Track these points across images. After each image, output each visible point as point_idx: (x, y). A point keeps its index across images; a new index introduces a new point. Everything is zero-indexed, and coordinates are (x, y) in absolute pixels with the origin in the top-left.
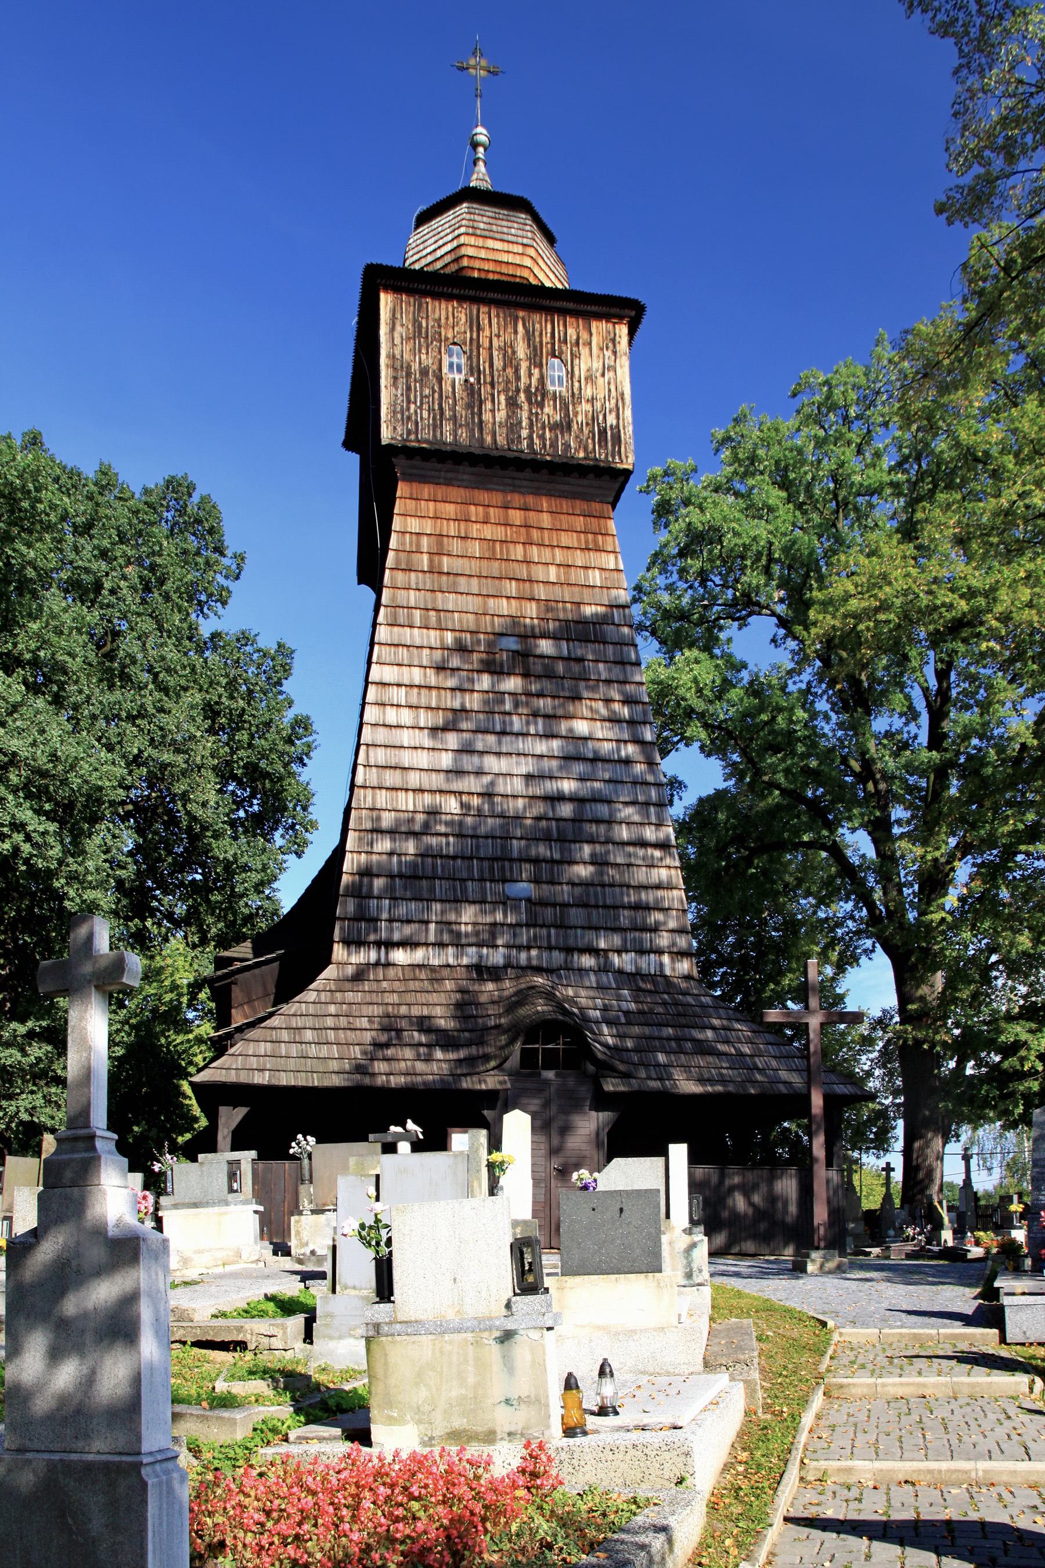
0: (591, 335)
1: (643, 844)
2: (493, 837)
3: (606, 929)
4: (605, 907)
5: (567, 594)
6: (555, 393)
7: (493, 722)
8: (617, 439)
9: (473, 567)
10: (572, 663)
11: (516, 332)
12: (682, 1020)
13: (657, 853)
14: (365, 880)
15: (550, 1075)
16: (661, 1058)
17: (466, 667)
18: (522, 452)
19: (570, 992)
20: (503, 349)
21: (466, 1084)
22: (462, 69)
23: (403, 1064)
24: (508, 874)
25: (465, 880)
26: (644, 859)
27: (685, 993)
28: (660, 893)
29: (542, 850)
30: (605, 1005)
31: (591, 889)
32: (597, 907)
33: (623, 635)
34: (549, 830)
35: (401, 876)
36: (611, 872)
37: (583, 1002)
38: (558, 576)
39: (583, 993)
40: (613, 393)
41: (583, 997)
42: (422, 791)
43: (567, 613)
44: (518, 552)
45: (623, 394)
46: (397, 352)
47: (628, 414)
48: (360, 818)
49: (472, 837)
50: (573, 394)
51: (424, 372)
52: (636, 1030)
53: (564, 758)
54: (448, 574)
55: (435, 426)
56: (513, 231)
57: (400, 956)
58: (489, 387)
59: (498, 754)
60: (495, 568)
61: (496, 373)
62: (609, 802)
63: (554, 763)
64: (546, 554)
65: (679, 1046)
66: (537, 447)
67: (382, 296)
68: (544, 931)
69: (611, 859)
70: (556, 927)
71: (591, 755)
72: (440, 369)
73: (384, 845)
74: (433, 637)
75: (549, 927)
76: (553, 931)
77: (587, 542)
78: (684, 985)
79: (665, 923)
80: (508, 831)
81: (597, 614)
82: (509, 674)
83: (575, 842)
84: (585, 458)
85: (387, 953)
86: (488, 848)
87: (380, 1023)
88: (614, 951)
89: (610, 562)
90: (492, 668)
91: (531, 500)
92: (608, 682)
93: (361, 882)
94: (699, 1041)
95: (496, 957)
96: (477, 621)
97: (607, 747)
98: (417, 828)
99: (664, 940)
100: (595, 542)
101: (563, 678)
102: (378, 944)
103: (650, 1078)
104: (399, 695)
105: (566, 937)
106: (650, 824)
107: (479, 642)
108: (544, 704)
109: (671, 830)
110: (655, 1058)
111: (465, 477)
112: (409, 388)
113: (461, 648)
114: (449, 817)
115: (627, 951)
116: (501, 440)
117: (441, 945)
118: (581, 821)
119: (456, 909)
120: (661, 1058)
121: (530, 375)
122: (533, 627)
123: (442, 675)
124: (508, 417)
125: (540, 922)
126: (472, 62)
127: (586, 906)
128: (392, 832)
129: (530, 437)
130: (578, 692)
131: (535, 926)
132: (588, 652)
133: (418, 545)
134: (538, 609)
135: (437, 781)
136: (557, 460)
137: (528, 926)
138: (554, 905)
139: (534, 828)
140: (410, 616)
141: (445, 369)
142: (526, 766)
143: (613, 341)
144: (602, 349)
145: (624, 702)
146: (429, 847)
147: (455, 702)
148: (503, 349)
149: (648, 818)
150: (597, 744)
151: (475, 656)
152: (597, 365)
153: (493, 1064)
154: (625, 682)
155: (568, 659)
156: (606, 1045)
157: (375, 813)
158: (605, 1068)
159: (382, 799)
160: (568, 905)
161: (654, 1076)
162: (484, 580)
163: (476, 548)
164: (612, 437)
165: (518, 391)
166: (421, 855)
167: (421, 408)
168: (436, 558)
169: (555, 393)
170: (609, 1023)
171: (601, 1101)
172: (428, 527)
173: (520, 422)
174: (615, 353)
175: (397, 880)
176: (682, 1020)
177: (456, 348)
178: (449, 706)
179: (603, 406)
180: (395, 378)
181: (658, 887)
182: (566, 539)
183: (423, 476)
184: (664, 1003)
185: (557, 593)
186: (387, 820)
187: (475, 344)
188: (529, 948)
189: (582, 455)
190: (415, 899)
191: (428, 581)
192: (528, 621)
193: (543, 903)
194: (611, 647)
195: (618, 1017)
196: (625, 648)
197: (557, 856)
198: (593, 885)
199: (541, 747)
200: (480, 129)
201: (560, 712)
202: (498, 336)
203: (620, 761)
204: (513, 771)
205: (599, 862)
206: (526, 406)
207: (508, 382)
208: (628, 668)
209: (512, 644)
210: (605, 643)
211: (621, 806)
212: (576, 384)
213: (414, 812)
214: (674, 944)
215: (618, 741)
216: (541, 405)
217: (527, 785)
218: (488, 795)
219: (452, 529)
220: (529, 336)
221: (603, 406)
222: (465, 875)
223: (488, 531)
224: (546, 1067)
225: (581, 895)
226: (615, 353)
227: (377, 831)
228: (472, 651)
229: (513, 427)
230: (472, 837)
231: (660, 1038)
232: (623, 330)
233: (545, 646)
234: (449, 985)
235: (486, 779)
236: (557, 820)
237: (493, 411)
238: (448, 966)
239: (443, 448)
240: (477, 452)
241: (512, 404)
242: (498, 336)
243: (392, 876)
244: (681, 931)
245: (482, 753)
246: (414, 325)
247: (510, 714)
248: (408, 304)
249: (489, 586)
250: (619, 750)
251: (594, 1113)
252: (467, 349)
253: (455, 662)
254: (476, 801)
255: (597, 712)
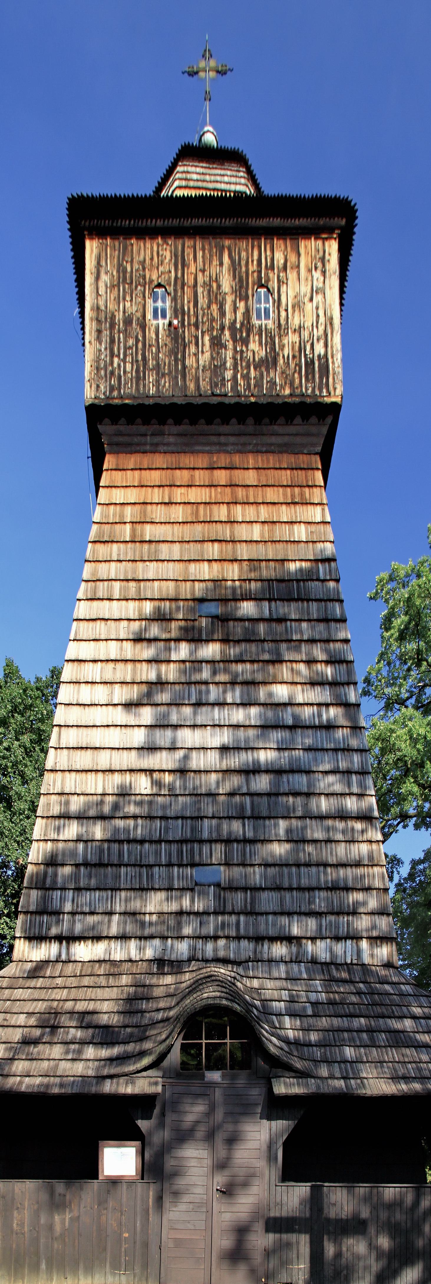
0: (299, 255)
1: (343, 816)
2: (183, 818)
3: (300, 914)
4: (300, 889)
5: (271, 552)
6: (260, 327)
7: (191, 692)
8: (325, 370)
9: (176, 532)
10: (274, 625)
11: (221, 264)
12: (379, 1010)
13: (358, 826)
14: (50, 870)
15: (215, 1076)
16: (349, 1052)
17: (164, 636)
18: (226, 395)
19: (256, 983)
20: (207, 285)
21: (108, 1087)
22: (193, 74)
23: (45, 1064)
24: (197, 859)
25: (151, 866)
26: (344, 832)
27: (384, 981)
28: (360, 871)
29: (236, 827)
30: (291, 996)
31: (286, 870)
32: (291, 889)
33: (328, 590)
34: (242, 807)
35: (86, 864)
36: (310, 848)
37: (268, 994)
38: (262, 534)
39: (269, 984)
40: (322, 319)
41: (267, 987)
42: (112, 771)
43: (268, 571)
44: (222, 513)
45: (332, 319)
46: (101, 303)
47: (337, 340)
48: (49, 804)
49: (161, 818)
50: (279, 325)
51: (128, 321)
52: (324, 1022)
53: (262, 727)
54: (150, 542)
55: (138, 378)
56: (226, 179)
57: (83, 951)
58: (193, 329)
59: (194, 726)
60: (198, 531)
61: (200, 312)
62: (308, 772)
63: (251, 732)
64: (250, 513)
65: (372, 1039)
66: (241, 389)
67: (88, 243)
68: (234, 918)
69: (309, 835)
70: (246, 914)
71: (290, 722)
72: (144, 316)
73: (72, 830)
74: (131, 609)
75: (238, 914)
76: (242, 918)
77: (293, 496)
78: (383, 972)
79: (365, 903)
80: (199, 809)
81: (301, 570)
82: (207, 641)
83: (269, 818)
84: (291, 395)
85: (68, 949)
86: (178, 830)
87: (38, 1020)
88: (307, 938)
89: (316, 514)
90: (193, 636)
91: (237, 459)
92: (312, 641)
93: (45, 874)
94: (398, 1031)
95: (182, 948)
96: (177, 588)
97: (307, 713)
98: (107, 809)
99: (363, 923)
100: (302, 495)
101: (264, 641)
102: (59, 938)
103: (332, 1077)
104: (93, 672)
105: (256, 925)
106: (351, 794)
107: (178, 609)
108: (243, 670)
109: (373, 800)
110: (342, 1053)
111: (172, 439)
112: (112, 341)
113: (160, 618)
114: (138, 798)
115: (322, 938)
116: (205, 386)
117: (123, 937)
118: (277, 795)
119: (141, 897)
120: (349, 1052)
121: (235, 309)
122: (234, 589)
123: (139, 646)
124: (212, 358)
125: (229, 908)
126: (202, 64)
127: (278, 889)
128: (81, 817)
129: (235, 378)
130: (279, 654)
131: (223, 913)
132: (292, 610)
133: (122, 515)
134: (241, 570)
135: (131, 760)
136: (263, 401)
137: (216, 913)
138: (245, 889)
139: (229, 805)
140: (110, 589)
141: (149, 316)
142: (224, 737)
143: (323, 259)
144: (310, 271)
145: (327, 662)
146: (116, 830)
147: (149, 673)
148: (207, 285)
149: (349, 787)
150: (297, 710)
151: (174, 625)
152: (305, 289)
153: (146, 1061)
154: (328, 641)
155: (270, 620)
156: (286, 1041)
157: (63, 798)
158: (279, 1066)
159: (71, 782)
160: (261, 889)
161: (338, 1075)
162: (186, 546)
163: (178, 513)
164: (319, 368)
165: (222, 328)
166: (108, 841)
167: (125, 363)
168: (138, 527)
169: (260, 327)
170: (293, 1015)
171: (276, 1107)
172: (132, 495)
173: (225, 363)
174: (324, 273)
175: (82, 869)
176: (379, 1010)
177: (160, 291)
178: (144, 679)
179: (311, 335)
180: (99, 332)
181: (358, 864)
182: (271, 495)
183: (130, 444)
184: (359, 993)
185: (260, 552)
186: (76, 804)
187: (179, 283)
188: (216, 938)
189: (287, 392)
190: (100, 889)
191: (129, 551)
192: (229, 583)
193: (232, 888)
194: (315, 604)
195: (304, 1008)
196: (330, 605)
197: (250, 834)
198: (287, 865)
199: (239, 715)
200: (208, 128)
201: (259, 677)
202: (203, 271)
203: (321, 727)
204: (204, 743)
205: (296, 839)
206: (230, 345)
207: (213, 320)
208: (333, 624)
209: (214, 609)
210: (308, 600)
211: (320, 775)
212: (283, 314)
213: (104, 795)
214: (374, 927)
215: (319, 705)
216: (246, 342)
217: (221, 759)
218: (182, 772)
219: (156, 495)
220: (235, 266)
221: (311, 335)
222: (152, 861)
223: (194, 495)
224: (209, 1068)
225: (274, 877)
226: (324, 273)
227: (66, 816)
228: (171, 620)
229: (217, 369)
230: (161, 818)
231: (349, 1030)
232: (333, 247)
233: (247, 608)
234: (125, 980)
235: (180, 754)
236: (251, 795)
237: (196, 355)
238: (131, 961)
239: (147, 402)
240: (180, 401)
241: (217, 343)
242: (203, 271)
243: (77, 865)
244: (381, 912)
245: (176, 727)
246: (118, 272)
247: (206, 683)
248: (113, 248)
249: (193, 551)
250: (320, 715)
251: (265, 1122)
252: (171, 289)
253: (155, 630)
254: (167, 778)
255: (299, 673)
